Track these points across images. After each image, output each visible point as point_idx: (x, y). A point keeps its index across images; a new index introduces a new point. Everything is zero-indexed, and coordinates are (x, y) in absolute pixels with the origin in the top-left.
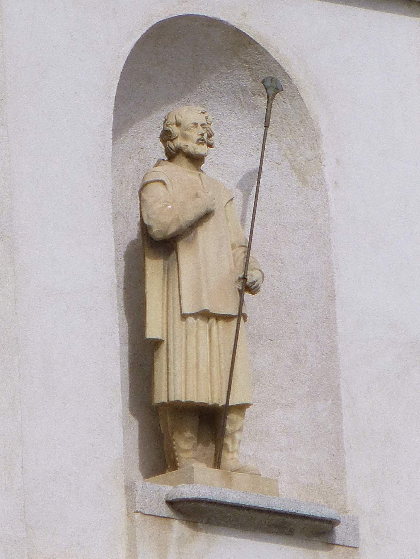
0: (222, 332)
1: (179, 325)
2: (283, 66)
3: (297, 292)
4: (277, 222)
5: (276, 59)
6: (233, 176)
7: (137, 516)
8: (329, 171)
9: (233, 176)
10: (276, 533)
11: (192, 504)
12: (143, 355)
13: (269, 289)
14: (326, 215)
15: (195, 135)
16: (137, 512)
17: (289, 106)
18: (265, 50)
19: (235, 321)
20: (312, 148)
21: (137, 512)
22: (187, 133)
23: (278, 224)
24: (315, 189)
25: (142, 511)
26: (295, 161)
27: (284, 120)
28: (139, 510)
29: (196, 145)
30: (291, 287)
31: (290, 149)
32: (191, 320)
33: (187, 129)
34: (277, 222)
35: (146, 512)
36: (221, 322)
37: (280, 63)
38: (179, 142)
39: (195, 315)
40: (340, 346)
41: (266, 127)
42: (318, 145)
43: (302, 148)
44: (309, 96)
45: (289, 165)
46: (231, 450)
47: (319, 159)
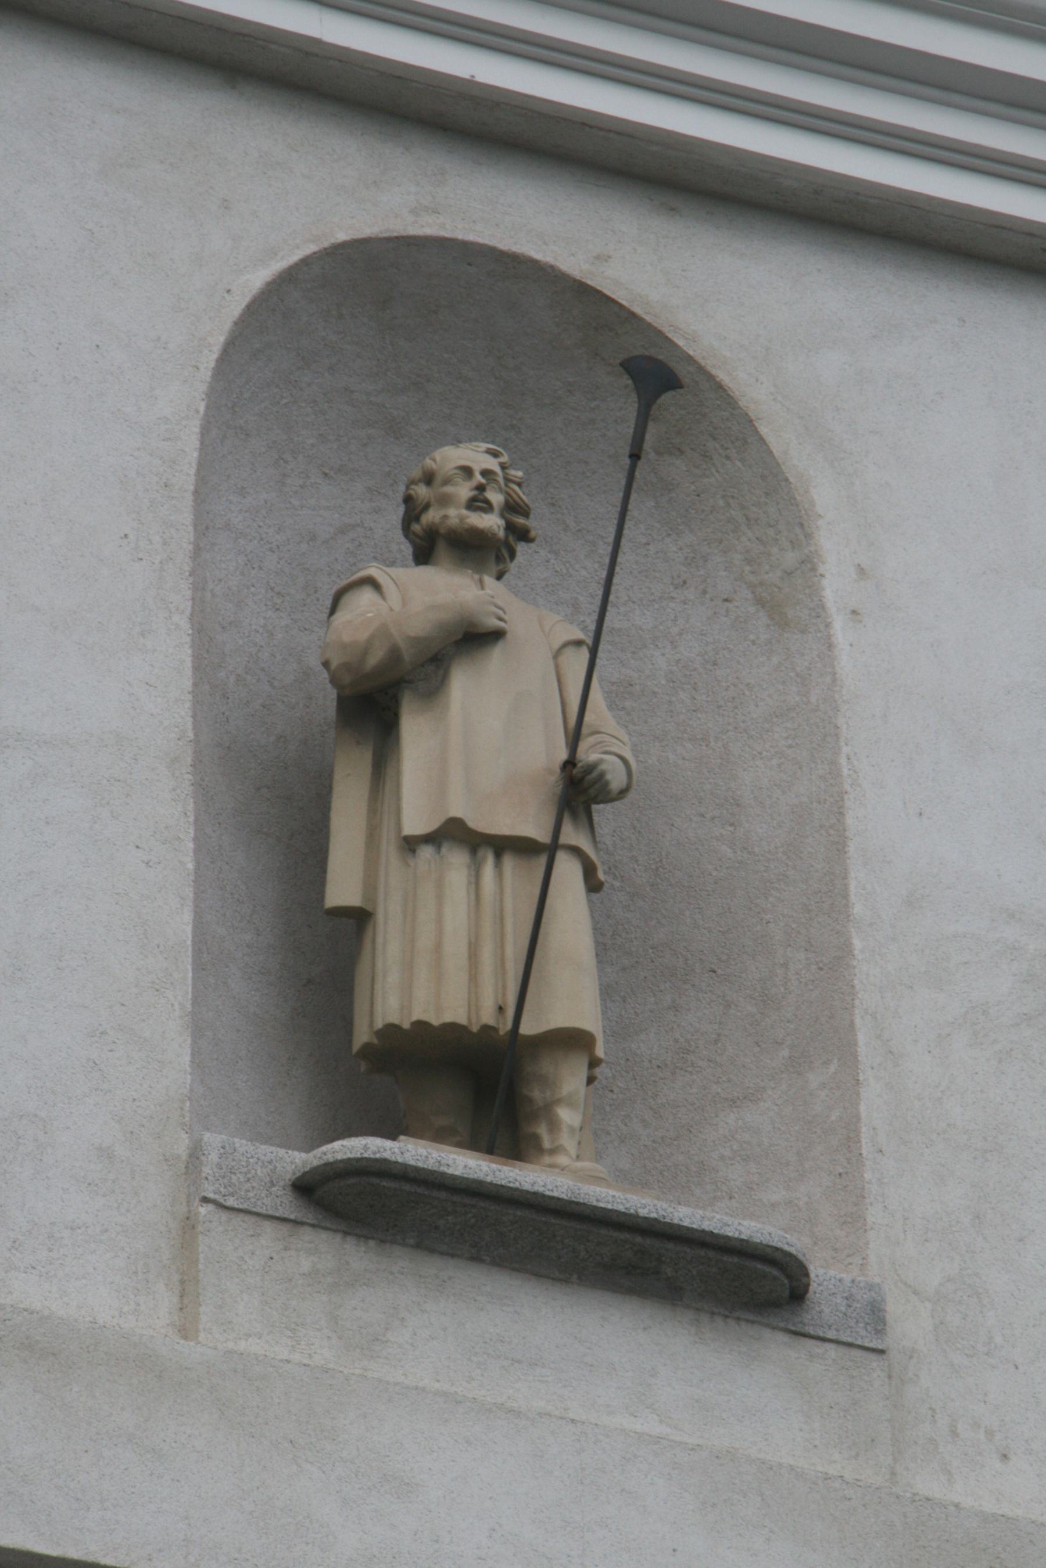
0: (511, 884)
1: (394, 871)
2: (709, 368)
3: (769, 856)
4: (729, 724)
5: (691, 353)
6: (633, 653)
7: (204, 1210)
8: (835, 585)
9: (633, 653)
10: (631, 1291)
11: (352, 1181)
12: (321, 949)
13: (710, 867)
14: (828, 679)
15: (464, 491)
16: (205, 1200)
17: (739, 464)
18: (660, 333)
19: (543, 860)
20: (794, 544)
21: (205, 1200)
22: (448, 489)
23: (730, 728)
24: (803, 632)
25: (217, 1197)
26: (761, 584)
27: (731, 501)
28: (211, 1196)
29: (464, 512)
30: (756, 849)
31: (749, 561)
32: (426, 852)
33: (447, 482)
34: (729, 724)
35: (231, 1202)
36: (509, 862)
37: (702, 362)
38: (432, 516)
39: (433, 839)
40: (857, 943)
41: (635, 456)
42: (809, 536)
43: (775, 550)
44: (782, 437)
45: (750, 596)
46: (547, 1144)
47: (809, 565)
